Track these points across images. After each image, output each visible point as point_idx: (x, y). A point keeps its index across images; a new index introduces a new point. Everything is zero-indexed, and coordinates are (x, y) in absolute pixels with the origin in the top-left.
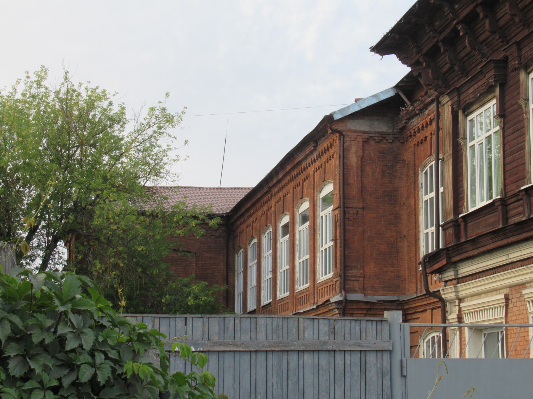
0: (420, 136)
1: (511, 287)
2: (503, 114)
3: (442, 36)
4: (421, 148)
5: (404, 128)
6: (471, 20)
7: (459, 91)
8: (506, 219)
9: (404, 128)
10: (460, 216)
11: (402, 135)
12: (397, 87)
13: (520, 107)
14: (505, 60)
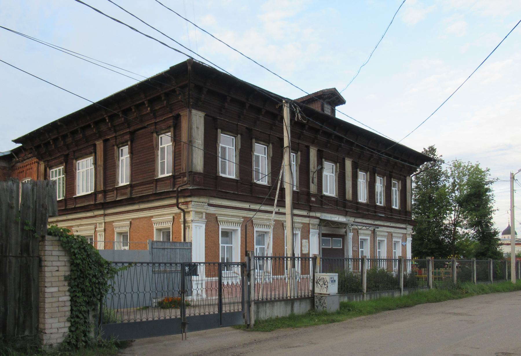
0: (21, 170)
1: (133, 219)
2: (66, 171)
3: (43, 142)
4: (21, 174)
5: (13, 166)
6: (55, 140)
7: (48, 161)
8: (66, 206)
9: (13, 166)
10: (455, 282)
11: (12, 168)
12: (12, 151)
13: (73, 171)
14: (68, 155)
